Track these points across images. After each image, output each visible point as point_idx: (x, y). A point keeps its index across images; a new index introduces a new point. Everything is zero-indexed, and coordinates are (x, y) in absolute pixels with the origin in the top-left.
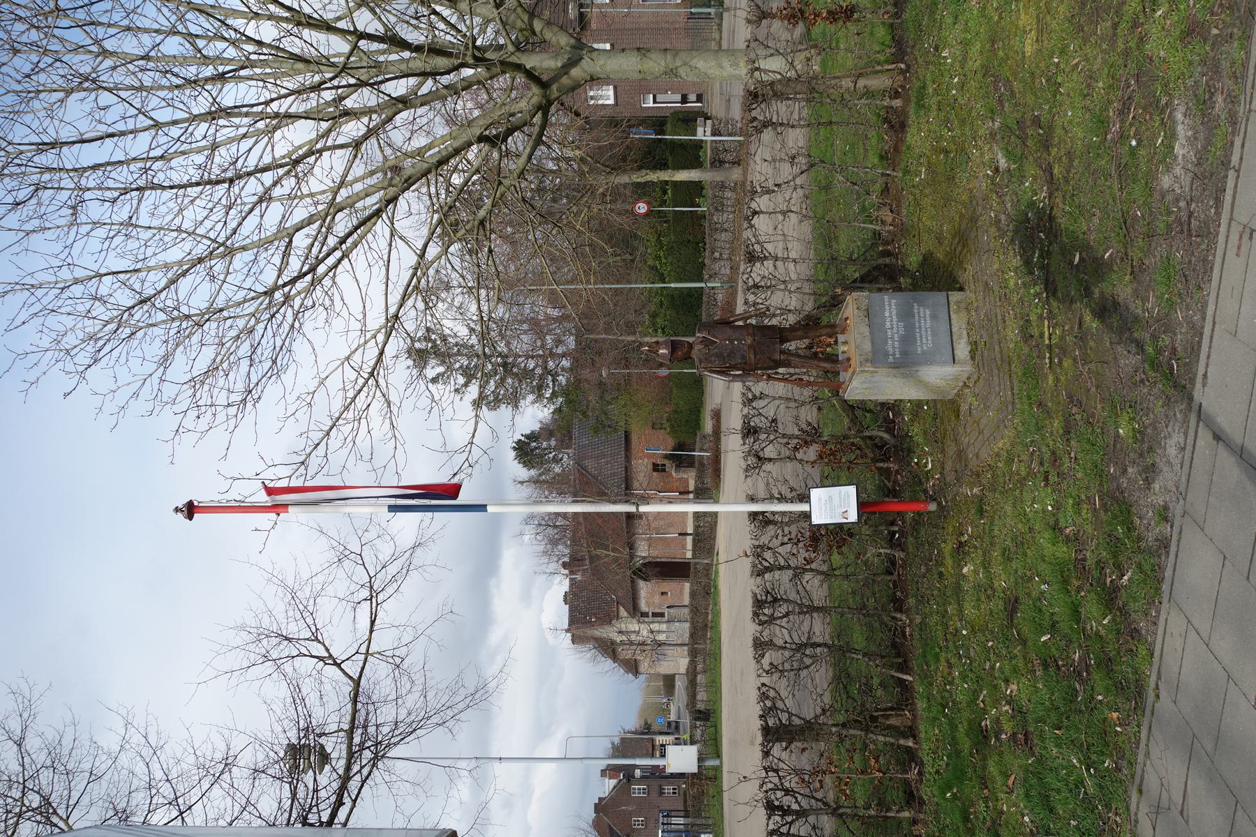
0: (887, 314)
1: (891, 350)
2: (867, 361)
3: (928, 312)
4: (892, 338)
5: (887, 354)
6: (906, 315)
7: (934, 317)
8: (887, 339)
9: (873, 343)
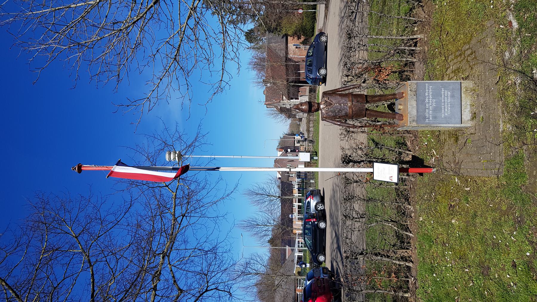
0: (427, 94)
1: (427, 115)
2: (413, 121)
3: (449, 94)
4: (429, 109)
5: (425, 118)
6: (437, 95)
7: (453, 96)
8: (426, 108)
9: (417, 111)
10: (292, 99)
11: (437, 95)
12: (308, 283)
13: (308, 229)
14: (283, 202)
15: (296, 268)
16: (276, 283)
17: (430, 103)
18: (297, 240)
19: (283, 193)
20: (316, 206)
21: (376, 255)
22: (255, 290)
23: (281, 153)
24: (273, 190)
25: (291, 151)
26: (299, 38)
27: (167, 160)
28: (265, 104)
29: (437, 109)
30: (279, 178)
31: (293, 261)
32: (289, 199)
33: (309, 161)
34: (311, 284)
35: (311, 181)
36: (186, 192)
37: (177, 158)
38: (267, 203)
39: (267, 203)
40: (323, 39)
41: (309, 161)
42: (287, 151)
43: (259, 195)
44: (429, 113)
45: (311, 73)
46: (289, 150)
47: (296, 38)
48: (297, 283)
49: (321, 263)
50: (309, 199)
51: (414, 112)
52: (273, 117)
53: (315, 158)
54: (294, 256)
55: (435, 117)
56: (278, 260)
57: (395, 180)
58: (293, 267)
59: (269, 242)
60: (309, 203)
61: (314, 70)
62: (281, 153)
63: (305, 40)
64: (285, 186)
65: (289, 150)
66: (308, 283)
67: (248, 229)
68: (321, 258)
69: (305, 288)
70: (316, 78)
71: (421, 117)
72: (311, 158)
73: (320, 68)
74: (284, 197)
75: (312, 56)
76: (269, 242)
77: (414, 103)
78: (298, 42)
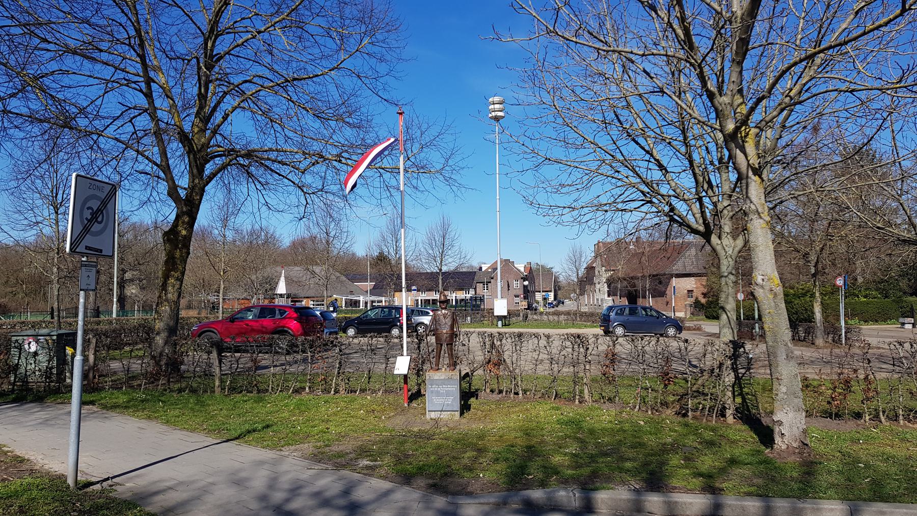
10: (609, 286)
11: (448, 394)
12: (318, 313)
13: (390, 312)
14: (433, 276)
15: (342, 300)
16: (317, 269)
17: (443, 389)
18: (383, 299)
19: (446, 275)
20: (422, 323)
21: (340, 363)
22: (306, 236)
23: (522, 270)
24: (450, 260)
25: (524, 286)
26: (705, 295)
27: (491, 100)
28: (599, 242)
29: (438, 394)
30: (481, 269)
31: (352, 293)
32: (437, 286)
33: (496, 314)
34: (316, 316)
35: (469, 318)
36: (420, 160)
37: (493, 114)
38: (431, 252)
39: (431, 252)
40: (671, 331)
41: (496, 314)
42: (524, 279)
43: (442, 240)
44: (435, 388)
45: (617, 314)
46: (526, 283)
47: (705, 291)
48: (319, 300)
49: (345, 331)
50: (431, 313)
51: (436, 378)
52: (570, 257)
53: (500, 323)
54: (359, 295)
55: (432, 392)
56: (351, 270)
57: (396, 372)
58: (342, 294)
59: (381, 254)
60: (427, 314)
61: (621, 318)
62: (522, 270)
63: (702, 305)
64: (464, 278)
65: (526, 283)
66: (318, 313)
67: (391, 227)
68: (351, 332)
69: (309, 308)
70: (609, 321)
71: (433, 382)
72: (500, 318)
73: (625, 328)
74: (441, 277)
75: (647, 315)
76: (381, 254)
77: (442, 378)
78: (698, 294)
